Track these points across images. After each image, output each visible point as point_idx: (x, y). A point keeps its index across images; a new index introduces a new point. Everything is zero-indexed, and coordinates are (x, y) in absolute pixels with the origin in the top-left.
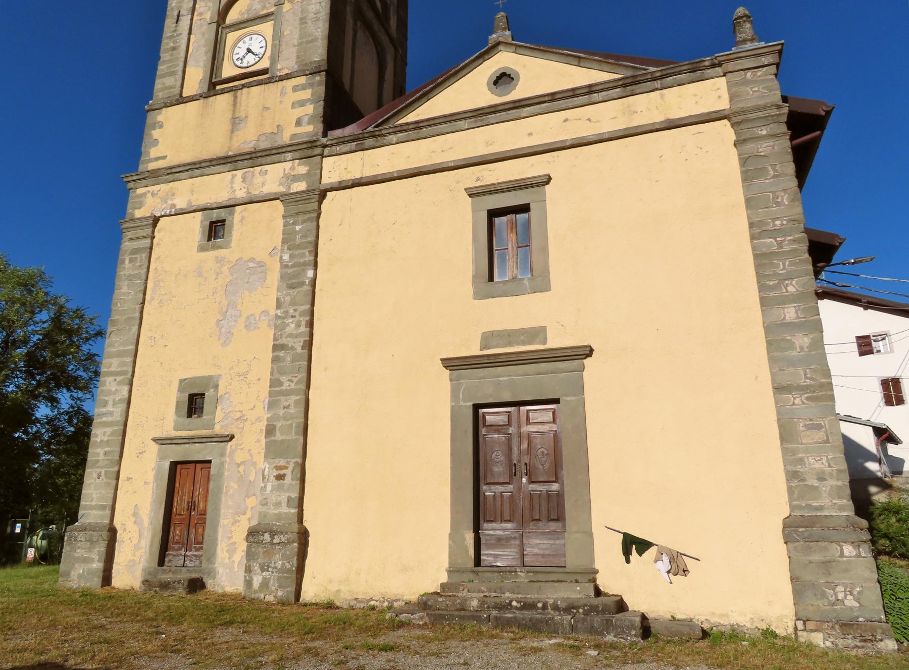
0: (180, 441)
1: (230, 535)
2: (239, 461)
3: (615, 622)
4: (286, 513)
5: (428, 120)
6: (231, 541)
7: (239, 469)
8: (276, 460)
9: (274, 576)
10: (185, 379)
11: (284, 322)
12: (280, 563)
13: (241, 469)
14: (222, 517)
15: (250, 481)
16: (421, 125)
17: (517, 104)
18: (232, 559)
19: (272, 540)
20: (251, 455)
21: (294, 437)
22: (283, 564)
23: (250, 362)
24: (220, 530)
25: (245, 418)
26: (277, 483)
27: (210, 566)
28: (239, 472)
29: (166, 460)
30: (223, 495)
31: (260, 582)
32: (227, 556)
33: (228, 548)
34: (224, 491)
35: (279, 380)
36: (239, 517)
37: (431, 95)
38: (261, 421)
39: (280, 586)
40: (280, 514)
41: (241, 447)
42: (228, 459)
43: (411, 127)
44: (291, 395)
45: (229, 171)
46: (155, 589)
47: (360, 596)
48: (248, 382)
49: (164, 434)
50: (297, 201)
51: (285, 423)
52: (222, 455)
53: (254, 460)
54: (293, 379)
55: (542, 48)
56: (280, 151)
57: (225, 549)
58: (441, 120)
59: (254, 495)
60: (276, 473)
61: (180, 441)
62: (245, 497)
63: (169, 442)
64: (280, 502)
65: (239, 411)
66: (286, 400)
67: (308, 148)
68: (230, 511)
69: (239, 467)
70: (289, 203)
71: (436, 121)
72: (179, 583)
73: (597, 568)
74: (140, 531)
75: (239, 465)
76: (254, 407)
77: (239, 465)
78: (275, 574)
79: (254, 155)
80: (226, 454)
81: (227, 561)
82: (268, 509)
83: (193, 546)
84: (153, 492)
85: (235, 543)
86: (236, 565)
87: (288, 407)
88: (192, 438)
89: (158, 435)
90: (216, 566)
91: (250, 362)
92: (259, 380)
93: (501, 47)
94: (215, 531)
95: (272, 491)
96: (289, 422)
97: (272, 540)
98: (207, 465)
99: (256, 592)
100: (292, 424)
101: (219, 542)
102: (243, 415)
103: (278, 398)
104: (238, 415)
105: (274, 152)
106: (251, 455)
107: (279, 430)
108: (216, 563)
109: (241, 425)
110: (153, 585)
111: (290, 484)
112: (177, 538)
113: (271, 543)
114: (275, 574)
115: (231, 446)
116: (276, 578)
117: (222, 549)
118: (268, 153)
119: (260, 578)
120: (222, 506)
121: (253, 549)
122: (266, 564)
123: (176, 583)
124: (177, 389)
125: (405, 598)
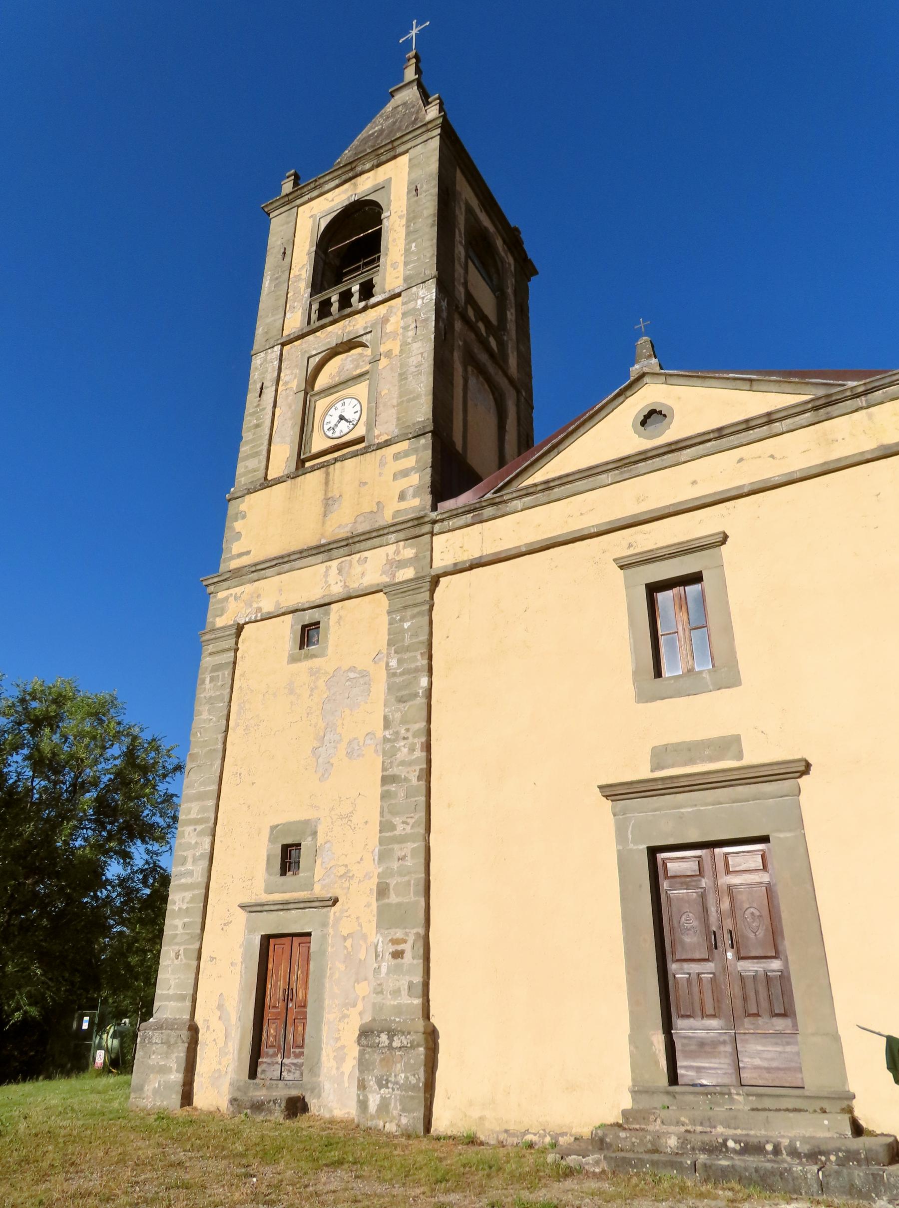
1: (337, 1036)
6: (339, 1044)
8: (392, 931)
12: (403, 1075)
13: (348, 943)
14: (326, 1010)
15: (360, 960)
16: (552, 484)
18: (341, 1070)
19: (391, 1043)
21: (413, 899)
22: (407, 1078)
25: (351, 875)
26: (393, 962)
28: (345, 947)
30: (327, 980)
33: (335, 1054)
34: (328, 974)
36: (348, 1010)
37: (561, 447)
39: (403, 1110)
40: (399, 1006)
42: (331, 931)
44: (408, 841)
47: (511, 1127)
50: (405, 592)
51: (399, 880)
52: (324, 925)
53: (364, 931)
54: (409, 820)
58: (577, 477)
59: (366, 980)
60: (392, 948)
61: (272, 908)
66: (401, 849)
70: (395, 595)
71: (570, 478)
73: (852, 1090)
74: (226, 1030)
75: (345, 939)
76: (361, 859)
77: (345, 939)
78: (396, 1092)
79: (350, 541)
81: (334, 1071)
82: (383, 999)
83: (292, 1050)
84: (241, 977)
90: (320, 1079)
92: (366, 823)
93: (646, 379)
94: (319, 1030)
95: (388, 973)
96: (406, 878)
99: (372, 1118)
100: (409, 881)
101: (324, 1046)
102: (348, 871)
104: (342, 870)
105: (374, 534)
106: (360, 925)
109: (346, 885)
113: (390, 1047)
114: (396, 1092)
117: (328, 1055)
118: (367, 536)
123: (272, 1103)
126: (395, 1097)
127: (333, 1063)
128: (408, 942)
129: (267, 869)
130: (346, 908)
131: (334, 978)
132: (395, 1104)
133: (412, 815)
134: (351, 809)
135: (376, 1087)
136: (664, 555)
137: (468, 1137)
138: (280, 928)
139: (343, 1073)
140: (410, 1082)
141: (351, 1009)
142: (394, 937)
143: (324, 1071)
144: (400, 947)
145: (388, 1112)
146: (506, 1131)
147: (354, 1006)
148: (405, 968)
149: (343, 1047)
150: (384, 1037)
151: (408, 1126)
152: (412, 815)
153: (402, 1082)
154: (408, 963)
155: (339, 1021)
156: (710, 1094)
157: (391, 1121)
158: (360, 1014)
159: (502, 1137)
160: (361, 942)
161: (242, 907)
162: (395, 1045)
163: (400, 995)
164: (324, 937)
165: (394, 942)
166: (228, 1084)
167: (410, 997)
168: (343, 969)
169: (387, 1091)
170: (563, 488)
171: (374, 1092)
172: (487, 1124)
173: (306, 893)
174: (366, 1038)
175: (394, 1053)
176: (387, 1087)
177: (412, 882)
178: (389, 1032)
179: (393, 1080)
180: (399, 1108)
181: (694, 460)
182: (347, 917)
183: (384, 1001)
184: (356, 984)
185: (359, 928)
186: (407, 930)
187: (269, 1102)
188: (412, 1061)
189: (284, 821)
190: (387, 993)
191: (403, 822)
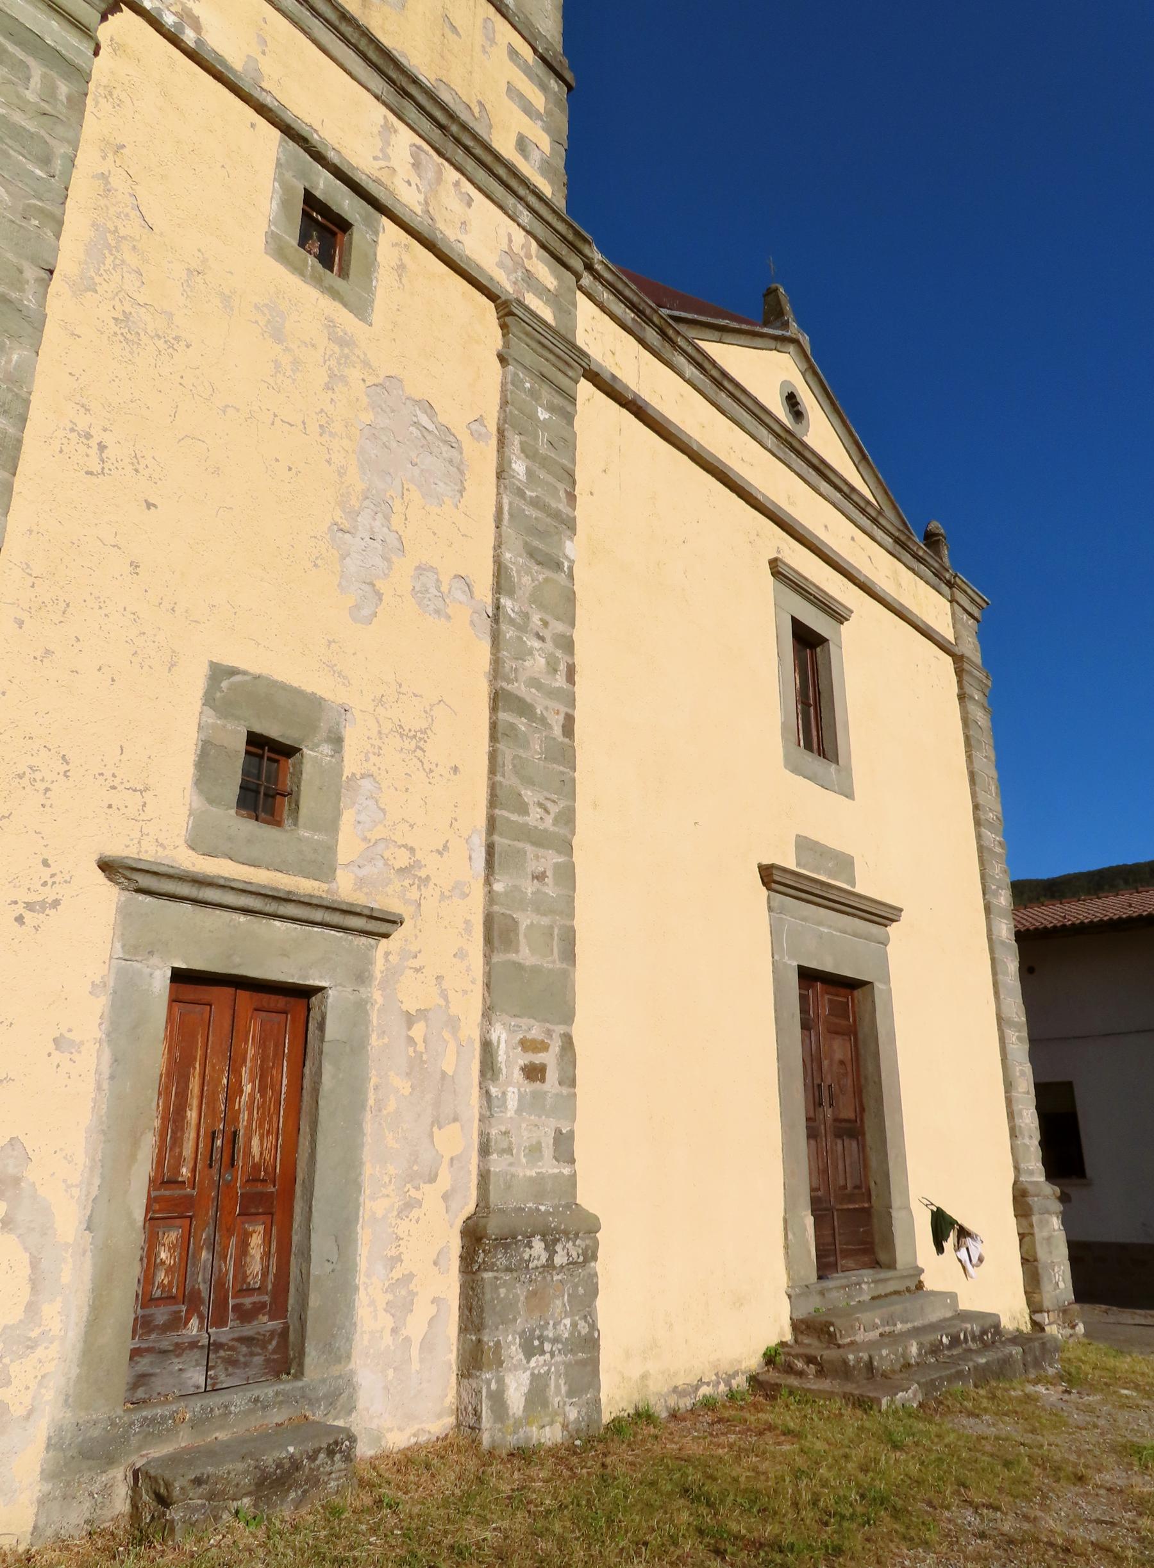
0: (230, 899)
1: (393, 1252)
2: (411, 1006)
3: (515, 1339)
4: (555, 1177)
5: (737, 385)
6: (397, 1274)
7: (411, 1033)
8: (524, 1022)
9: (556, 1365)
10: (233, 672)
11: (520, 638)
12: (567, 1321)
13: (418, 1031)
14: (367, 1190)
15: (444, 1074)
16: (726, 383)
17: (822, 467)
18: (404, 1332)
19: (551, 1258)
20: (444, 995)
21: (558, 965)
22: (574, 1325)
23: (432, 706)
24: (364, 1235)
25: (422, 873)
26: (530, 1087)
27: (335, 1370)
28: (411, 1040)
29: (155, 960)
30: (368, 1116)
31: (525, 1389)
32: (389, 1322)
33: (390, 1297)
34: (371, 1102)
35: (520, 795)
36: (417, 1188)
37: (729, 337)
38: (465, 896)
39: (571, 1393)
40: (540, 1179)
41: (415, 963)
42: (377, 996)
43: (714, 373)
44: (548, 848)
45: (377, 98)
46: (235, 1505)
47: (680, 1382)
48: (427, 766)
49: (148, 852)
50: (544, 346)
51: (536, 919)
52: (362, 977)
53: (453, 1011)
54: (549, 805)
55: (837, 403)
56: (513, 183)
57: (382, 1299)
58: (749, 403)
59: (455, 1119)
60: (523, 1059)
61: (230, 899)
62: (432, 1125)
63: (185, 890)
64: (539, 1143)
65: (405, 846)
66: (537, 857)
67: (564, 239)
68: (391, 1169)
69: (409, 1028)
70: (527, 334)
71: (743, 398)
72: (331, 1453)
73: (920, 1266)
74: (34, 1264)
75: (409, 1020)
76: (445, 847)
77: (409, 1020)
78: (558, 1358)
79: (454, 128)
80: (371, 977)
81: (388, 1340)
82: (511, 1164)
83: (231, 1302)
84: (99, 1088)
85: (409, 1277)
86: (415, 1352)
87: (540, 877)
88: (286, 899)
89: (117, 849)
90: (352, 1366)
91: (432, 706)
92: (455, 769)
93: (792, 348)
94: (344, 1241)
95: (519, 1111)
96: (545, 921)
97: (551, 1258)
98: (298, 1004)
99: (518, 1424)
100: (551, 927)
101: (361, 1279)
102: (418, 864)
103: (520, 845)
104: (402, 859)
105: (502, 172)
106: (444, 995)
107: (525, 936)
108: (354, 1353)
109: (414, 894)
110: (232, 1491)
111: (557, 1095)
112: (161, 1276)
113: (549, 1266)
114: (558, 1358)
115: (387, 954)
116: (562, 1368)
117: (372, 1303)
118: (488, 159)
119: (525, 1377)
120: (367, 1154)
121: (502, 1291)
122: (537, 1332)
123: (322, 1456)
124: (200, 693)
125: (743, 1366)
126: (557, 1370)
127: (387, 1321)
128: (550, 1049)
129: (198, 782)
130: (414, 948)
131: (385, 1112)
132: (557, 1381)
133: (554, 797)
134: (424, 725)
135: (521, 1356)
136: (811, 594)
137: (354, 1436)
138: (237, 960)
139: (407, 1340)
140: (579, 1333)
141: (426, 1187)
142: (529, 1037)
143: (362, 1341)
144: (538, 1058)
145: (545, 1403)
146: (675, 1389)
147: (432, 1179)
148: (549, 1101)
149: (409, 1277)
150: (538, 1245)
151: (580, 1422)
152: (554, 797)
153: (566, 1335)
154: (554, 1091)
155: (398, 1216)
156: (848, 1286)
157: (552, 1423)
158: (446, 1197)
159: (672, 1401)
160: (447, 1035)
161: (108, 867)
162: (560, 1259)
163: (541, 1158)
164: (361, 1007)
165: (527, 1045)
166: (41, 1443)
167: (557, 1160)
168: (407, 1091)
169: (541, 1359)
170: (729, 400)
171: (516, 1368)
172: (651, 1383)
173: (316, 884)
174: (506, 1253)
175: (549, 1278)
176: (543, 1353)
177: (556, 931)
178: (544, 1236)
179: (551, 1335)
180: (564, 1389)
181: (826, 499)
182: (418, 970)
183: (513, 1170)
184: (435, 1129)
185: (442, 1002)
186: (551, 1027)
187: (312, 1458)
188: (581, 1291)
189: (255, 669)
190: (518, 1153)
191: (540, 805)
